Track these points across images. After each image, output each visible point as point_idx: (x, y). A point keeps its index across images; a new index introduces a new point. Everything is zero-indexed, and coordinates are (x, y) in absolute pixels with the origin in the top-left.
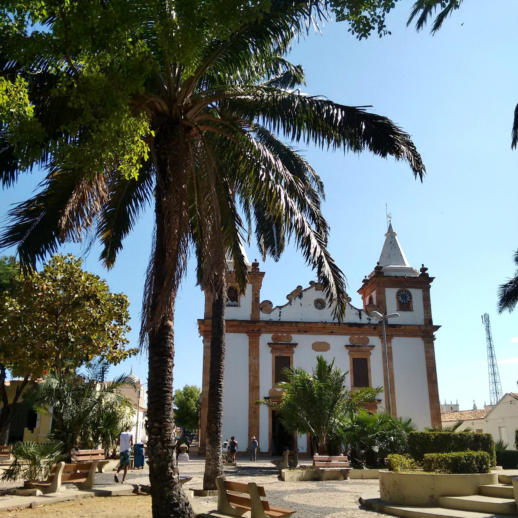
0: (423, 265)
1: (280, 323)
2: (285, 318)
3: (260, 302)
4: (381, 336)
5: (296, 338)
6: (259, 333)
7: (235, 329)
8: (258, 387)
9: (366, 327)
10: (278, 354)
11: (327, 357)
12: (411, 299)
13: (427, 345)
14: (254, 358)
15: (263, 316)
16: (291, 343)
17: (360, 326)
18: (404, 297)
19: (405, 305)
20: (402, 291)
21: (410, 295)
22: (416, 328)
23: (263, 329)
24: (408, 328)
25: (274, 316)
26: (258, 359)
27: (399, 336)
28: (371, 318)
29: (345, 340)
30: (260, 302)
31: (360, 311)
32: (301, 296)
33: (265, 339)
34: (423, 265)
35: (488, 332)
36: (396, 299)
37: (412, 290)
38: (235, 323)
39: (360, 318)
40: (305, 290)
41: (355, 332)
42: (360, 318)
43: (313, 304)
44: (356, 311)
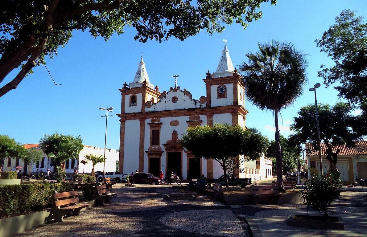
0: (209, 71)
1: (154, 112)
2: (158, 109)
3: (146, 102)
4: (207, 115)
5: (162, 120)
6: (145, 119)
7: (134, 117)
8: (144, 146)
9: (197, 110)
10: (153, 129)
11: (177, 128)
12: (226, 90)
13: (233, 117)
14: (142, 132)
15: (147, 110)
16: (160, 122)
17: (193, 109)
18: (222, 90)
19: (222, 94)
20: (221, 86)
21: (225, 88)
22: (226, 108)
23: (147, 116)
24: (221, 108)
25: (152, 109)
26: (144, 132)
27: (217, 113)
28: (202, 105)
29: (187, 118)
30: (146, 102)
31: (196, 101)
32: (165, 97)
33: (148, 121)
34: (125, 82)
35: (316, 98)
36: (217, 92)
37: (226, 85)
38: (133, 115)
39: (196, 105)
40: (167, 93)
41: (192, 113)
42: (196, 105)
43: (171, 100)
44: (194, 102)
